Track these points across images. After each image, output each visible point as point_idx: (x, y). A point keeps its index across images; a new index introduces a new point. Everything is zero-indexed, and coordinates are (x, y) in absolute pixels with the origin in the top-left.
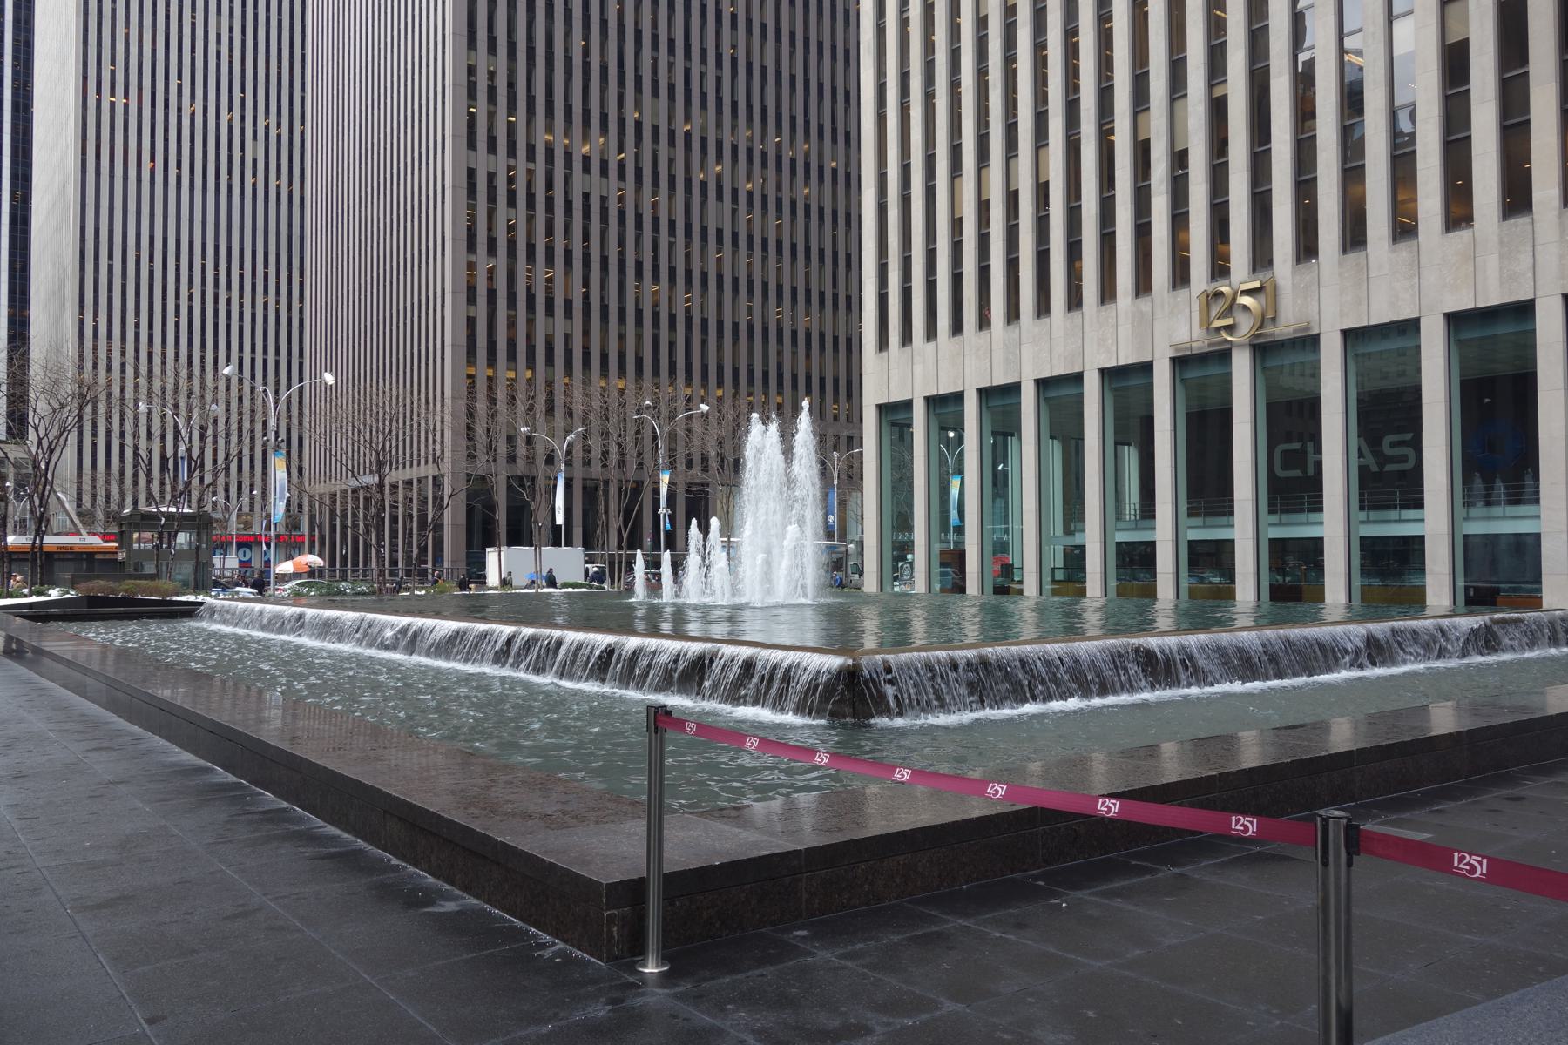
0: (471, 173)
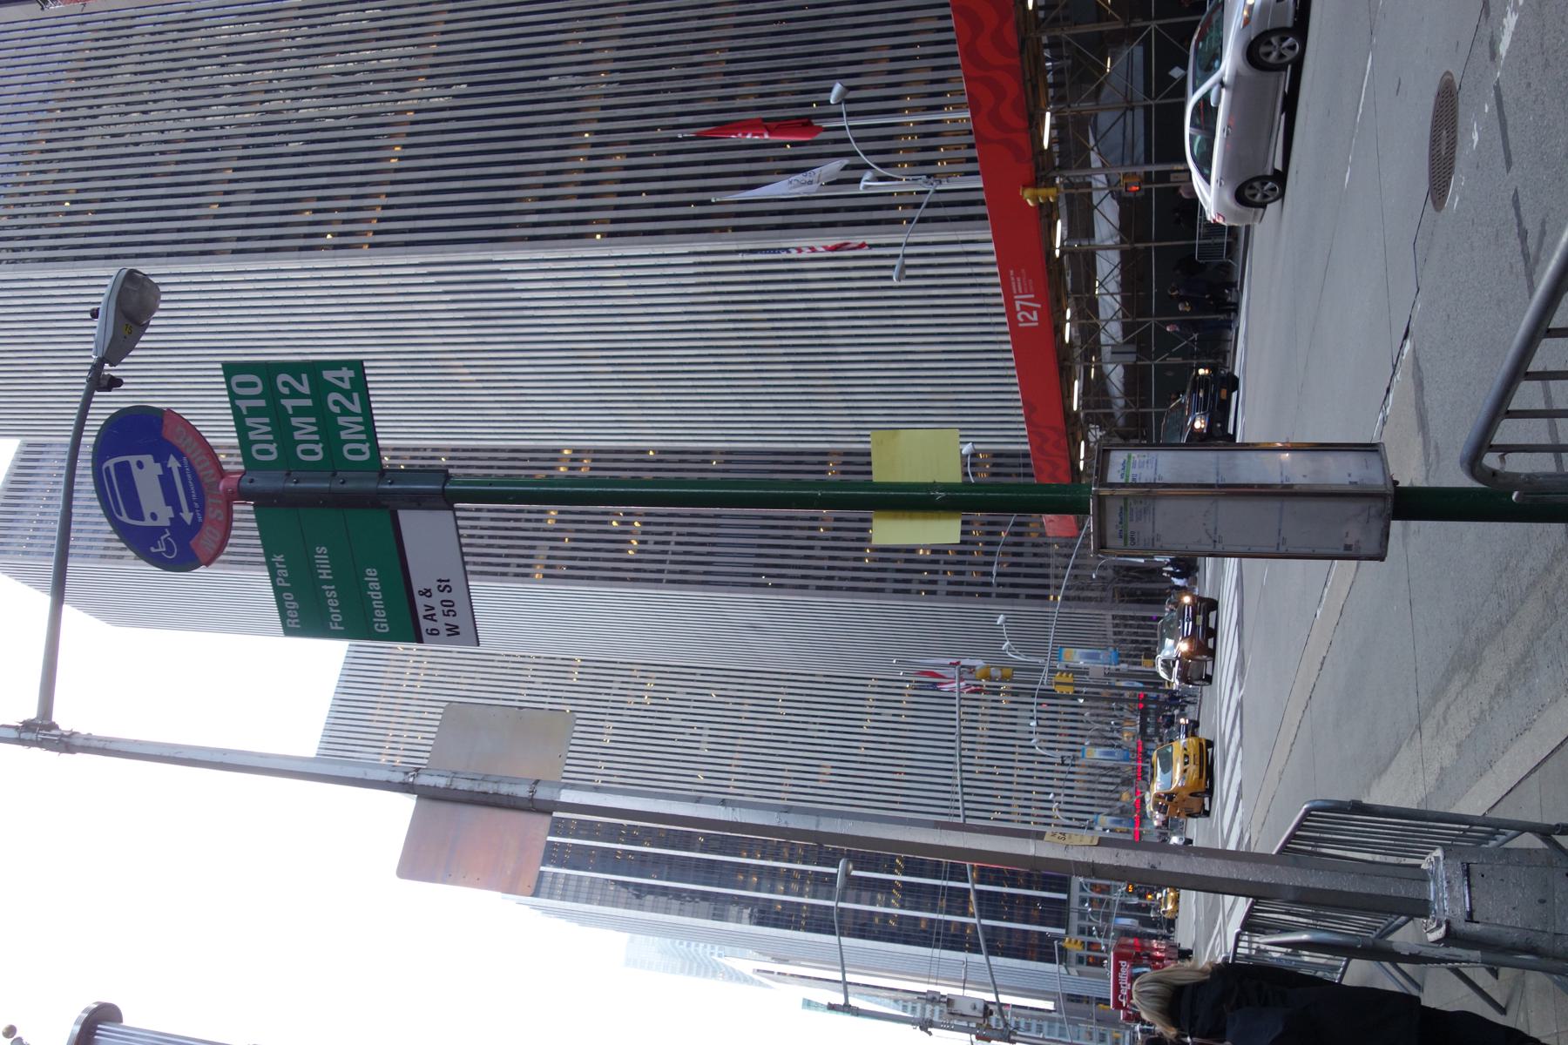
0: (948, 593)
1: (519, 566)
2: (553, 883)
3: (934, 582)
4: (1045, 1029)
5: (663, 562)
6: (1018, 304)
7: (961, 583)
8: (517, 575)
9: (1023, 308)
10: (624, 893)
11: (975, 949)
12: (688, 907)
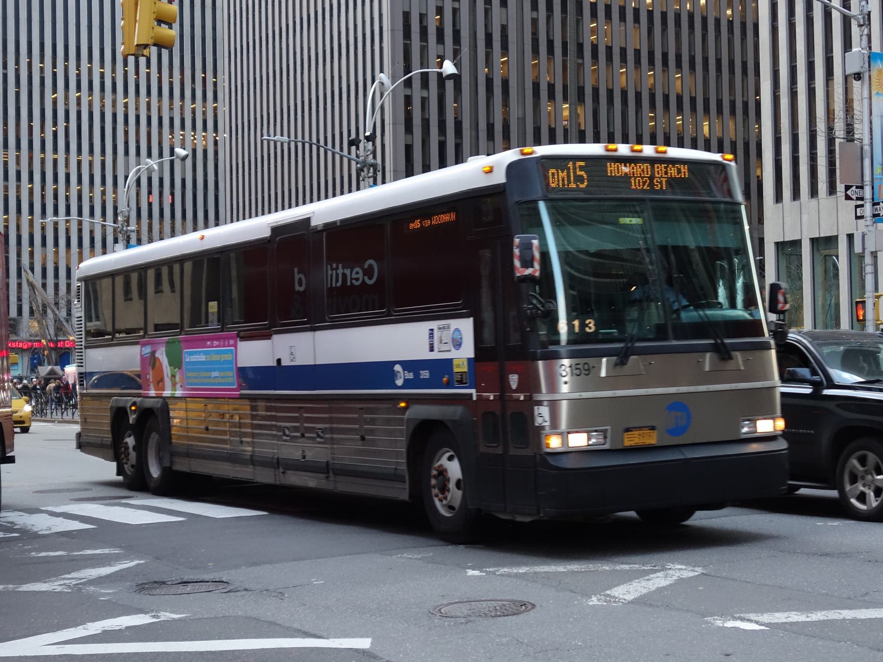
0: (407, 16)
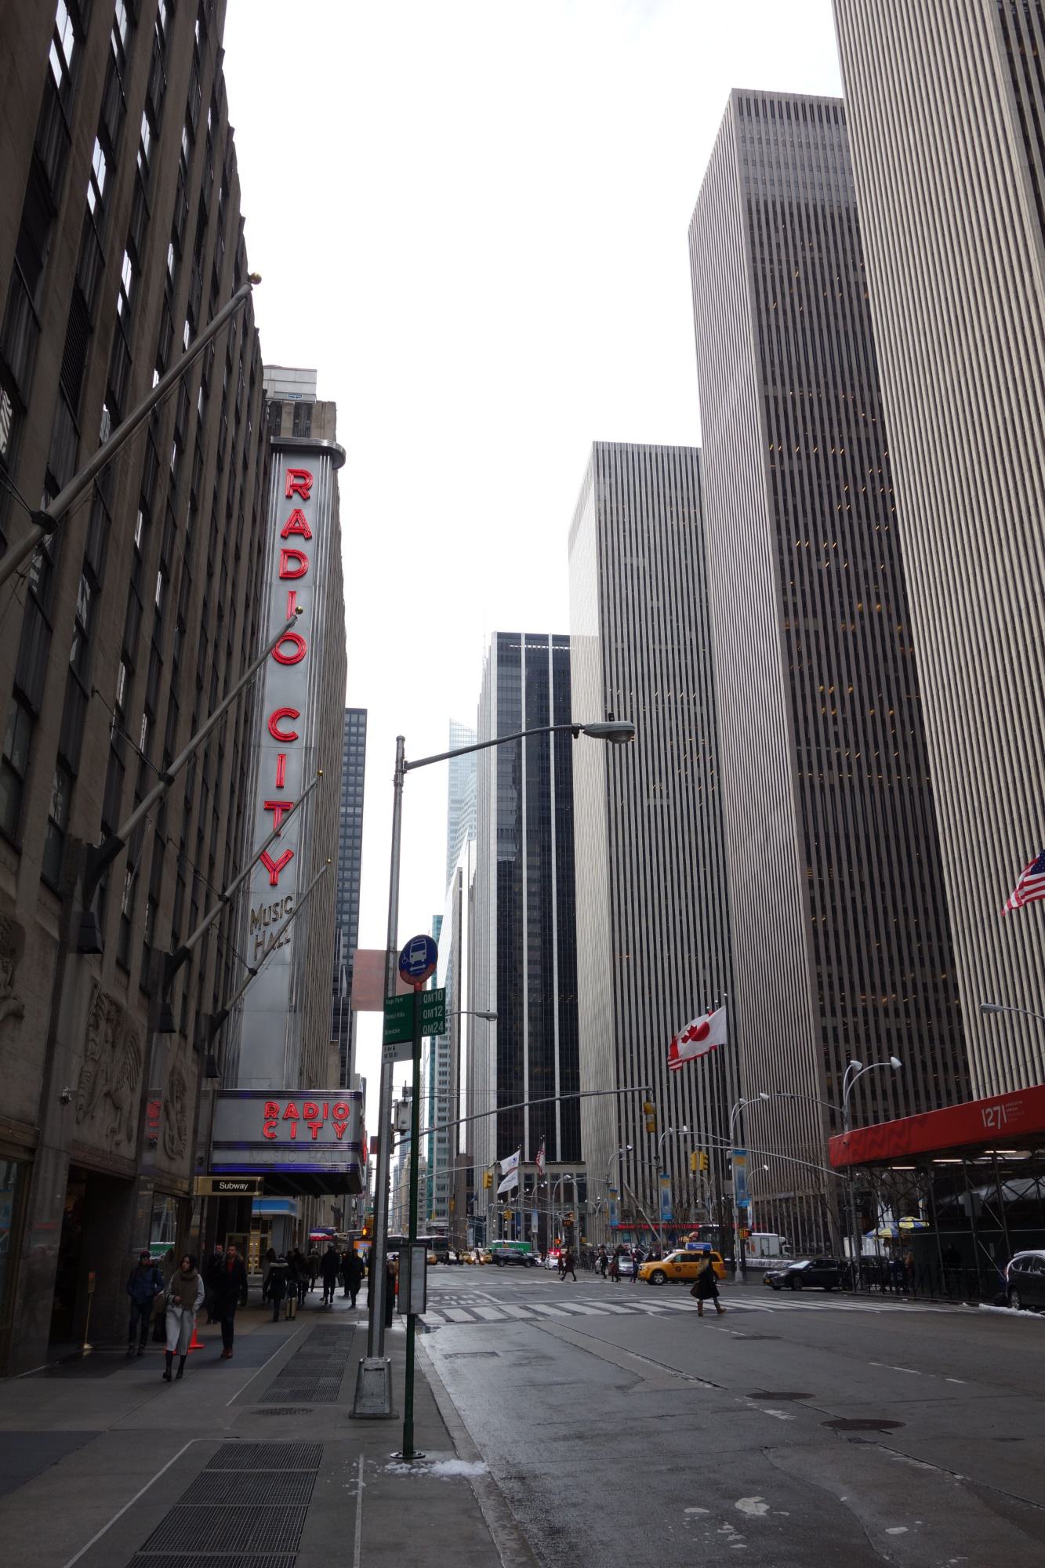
0: (824, 1029)
1: (795, 604)
2: (512, 677)
3: (834, 1014)
4: (442, 1146)
5: (818, 743)
6: (997, 1108)
7: (876, 1014)
8: (785, 604)
9: (996, 1113)
10: (512, 819)
11: (501, 1102)
12: (507, 1268)
